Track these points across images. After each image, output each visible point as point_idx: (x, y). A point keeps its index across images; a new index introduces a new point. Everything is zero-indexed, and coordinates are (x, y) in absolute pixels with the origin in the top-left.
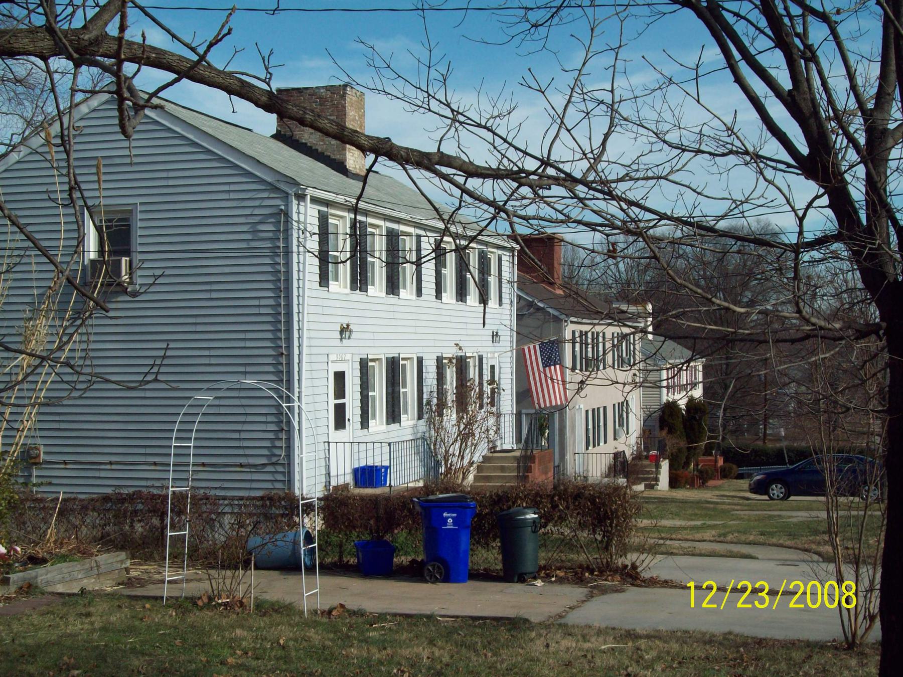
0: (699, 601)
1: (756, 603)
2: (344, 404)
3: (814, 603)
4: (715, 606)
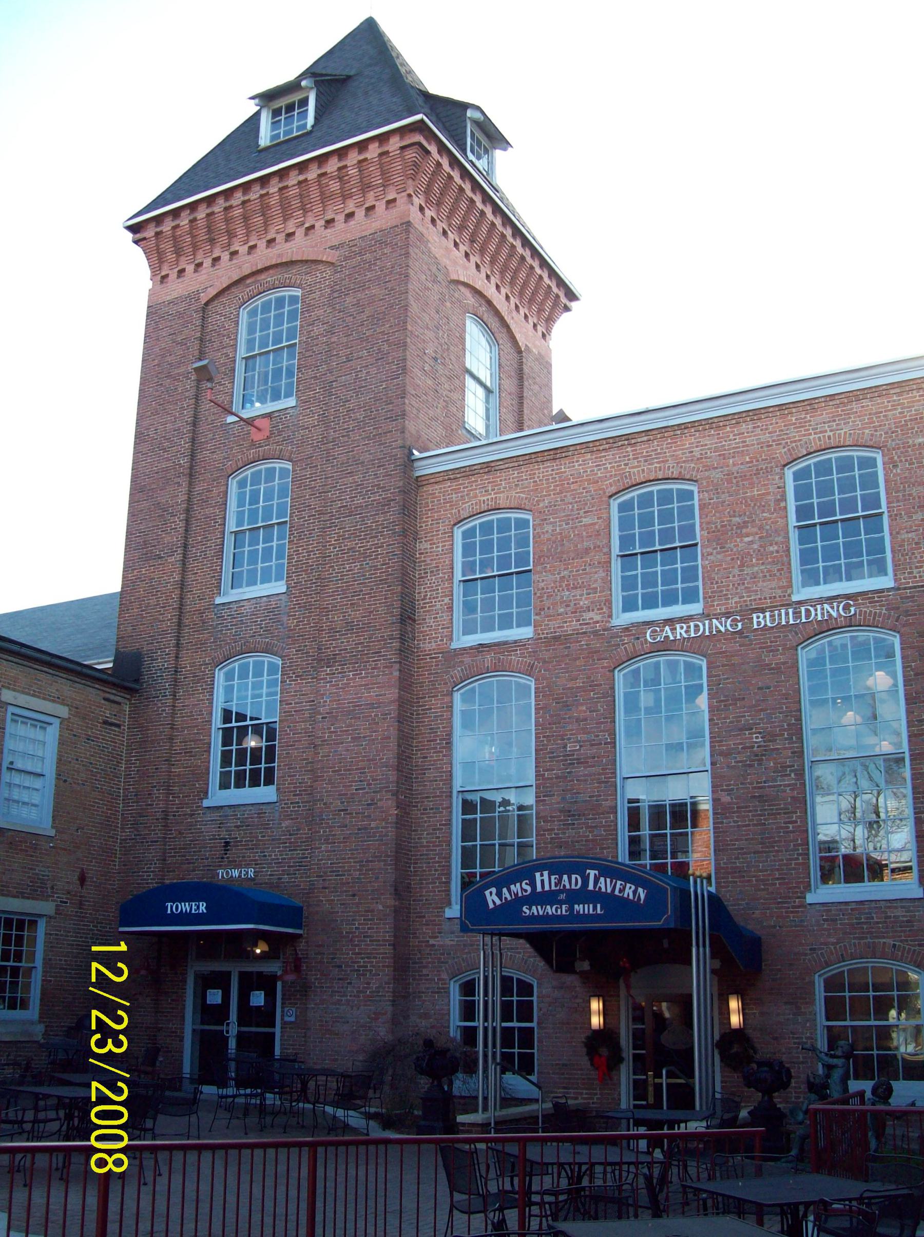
0: (100, 958)
1: (98, 1036)
2: (463, 814)
3: (99, 1115)
4: (94, 979)
